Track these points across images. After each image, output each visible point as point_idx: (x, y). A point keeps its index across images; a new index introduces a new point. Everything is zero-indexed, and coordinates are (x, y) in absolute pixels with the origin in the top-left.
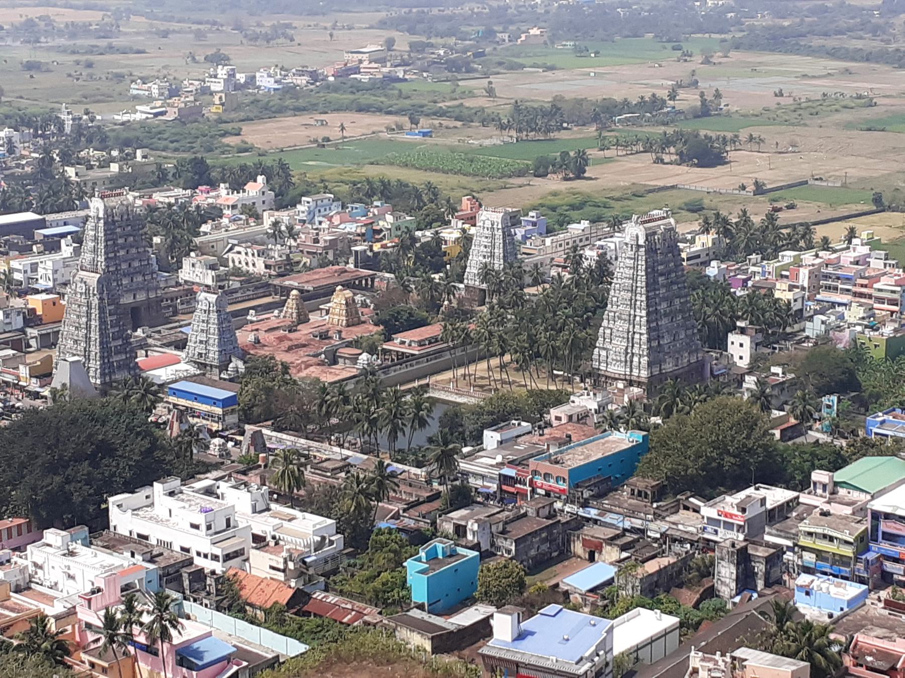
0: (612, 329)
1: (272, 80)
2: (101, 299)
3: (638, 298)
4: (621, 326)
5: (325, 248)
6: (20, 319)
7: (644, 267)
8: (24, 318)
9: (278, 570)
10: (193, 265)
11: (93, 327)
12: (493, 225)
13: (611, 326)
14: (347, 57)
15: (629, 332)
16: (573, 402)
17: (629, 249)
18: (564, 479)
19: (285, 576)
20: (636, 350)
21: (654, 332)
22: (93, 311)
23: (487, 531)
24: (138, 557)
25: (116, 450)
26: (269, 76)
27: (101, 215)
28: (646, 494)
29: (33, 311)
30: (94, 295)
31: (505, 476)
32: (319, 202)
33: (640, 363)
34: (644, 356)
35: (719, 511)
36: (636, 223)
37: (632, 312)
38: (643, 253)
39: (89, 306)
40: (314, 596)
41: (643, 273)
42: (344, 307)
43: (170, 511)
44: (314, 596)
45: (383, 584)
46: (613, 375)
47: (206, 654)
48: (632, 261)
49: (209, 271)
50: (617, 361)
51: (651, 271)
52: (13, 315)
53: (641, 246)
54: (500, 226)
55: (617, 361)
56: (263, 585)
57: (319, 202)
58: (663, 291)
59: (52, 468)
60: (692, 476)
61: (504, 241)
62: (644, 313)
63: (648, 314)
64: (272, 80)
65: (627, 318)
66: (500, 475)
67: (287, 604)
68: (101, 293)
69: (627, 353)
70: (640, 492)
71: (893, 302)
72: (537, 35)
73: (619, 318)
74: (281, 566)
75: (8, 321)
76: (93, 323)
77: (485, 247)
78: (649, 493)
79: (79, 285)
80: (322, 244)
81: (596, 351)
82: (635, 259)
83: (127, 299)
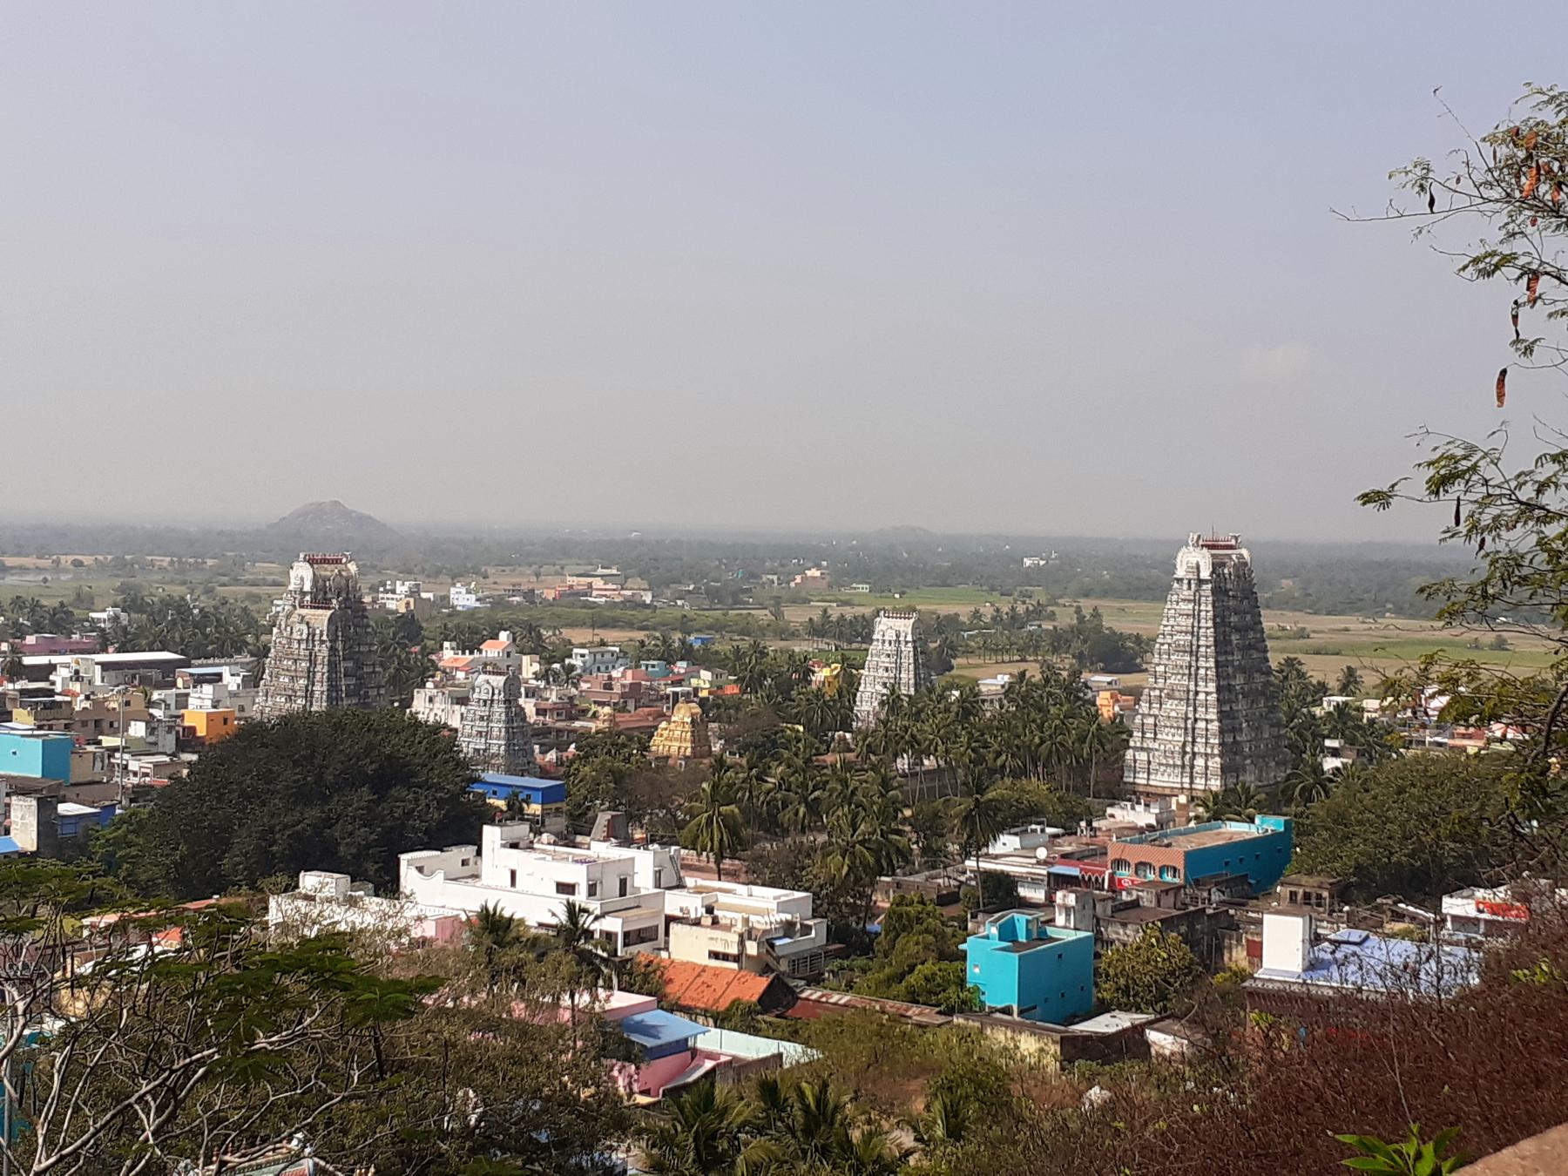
0: (1156, 717)
1: (473, 597)
2: (333, 650)
3: (1202, 663)
5: (623, 695)
6: (172, 738)
7: (1210, 614)
8: (177, 739)
9: (725, 957)
10: (431, 700)
11: (317, 694)
14: (571, 580)
15: (1187, 719)
16: (1112, 816)
17: (1185, 587)
18: (1175, 869)
20: (1200, 748)
22: (319, 668)
23: (1089, 912)
25: (414, 774)
26: (469, 592)
27: (307, 588)
28: (1319, 897)
29: (193, 729)
30: (322, 642)
31: (1057, 876)
32: (599, 657)
33: (1207, 768)
34: (1213, 756)
35: (1478, 903)
37: (1192, 687)
38: (1209, 593)
39: (312, 660)
40: (804, 995)
41: (1210, 624)
42: (688, 727)
43: (513, 874)
44: (804, 995)
45: (926, 979)
46: (1160, 791)
47: (664, 1030)
48: (1191, 606)
49: (457, 707)
50: (1167, 765)
51: (1220, 622)
52: (161, 731)
53: (1206, 582)
54: (909, 638)
55: (1167, 765)
56: (704, 977)
57: (599, 657)
58: (1237, 657)
59: (301, 796)
60: (1399, 863)
61: (916, 660)
62: (1212, 687)
63: (1219, 689)
64: (473, 597)
65: (1184, 696)
66: (1049, 874)
67: (760, 1000)
68: (333, 641)
69: (1185, 753)
70: (1307, 896)
72: (814, 578)
73: (1169, 697)
74: (734, 950)
75: (152, 739)
76: (317, 687)
77: (887, 669)
78: (1325, 894)
80: (617, 689)
81: (1129, 754)
82: (1196, 601)
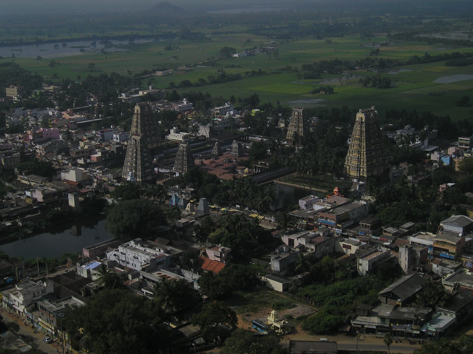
4: (355, 155)
9: (218, 257)
12: (298, 114)
13: (351, 156)
19: (221, 259)
20: (361, 166)
21: (369, 159)
24: (162, 251)
36: (16, 40)
71: (466, 145)
79: (133, 141)
83: (150, 147)
